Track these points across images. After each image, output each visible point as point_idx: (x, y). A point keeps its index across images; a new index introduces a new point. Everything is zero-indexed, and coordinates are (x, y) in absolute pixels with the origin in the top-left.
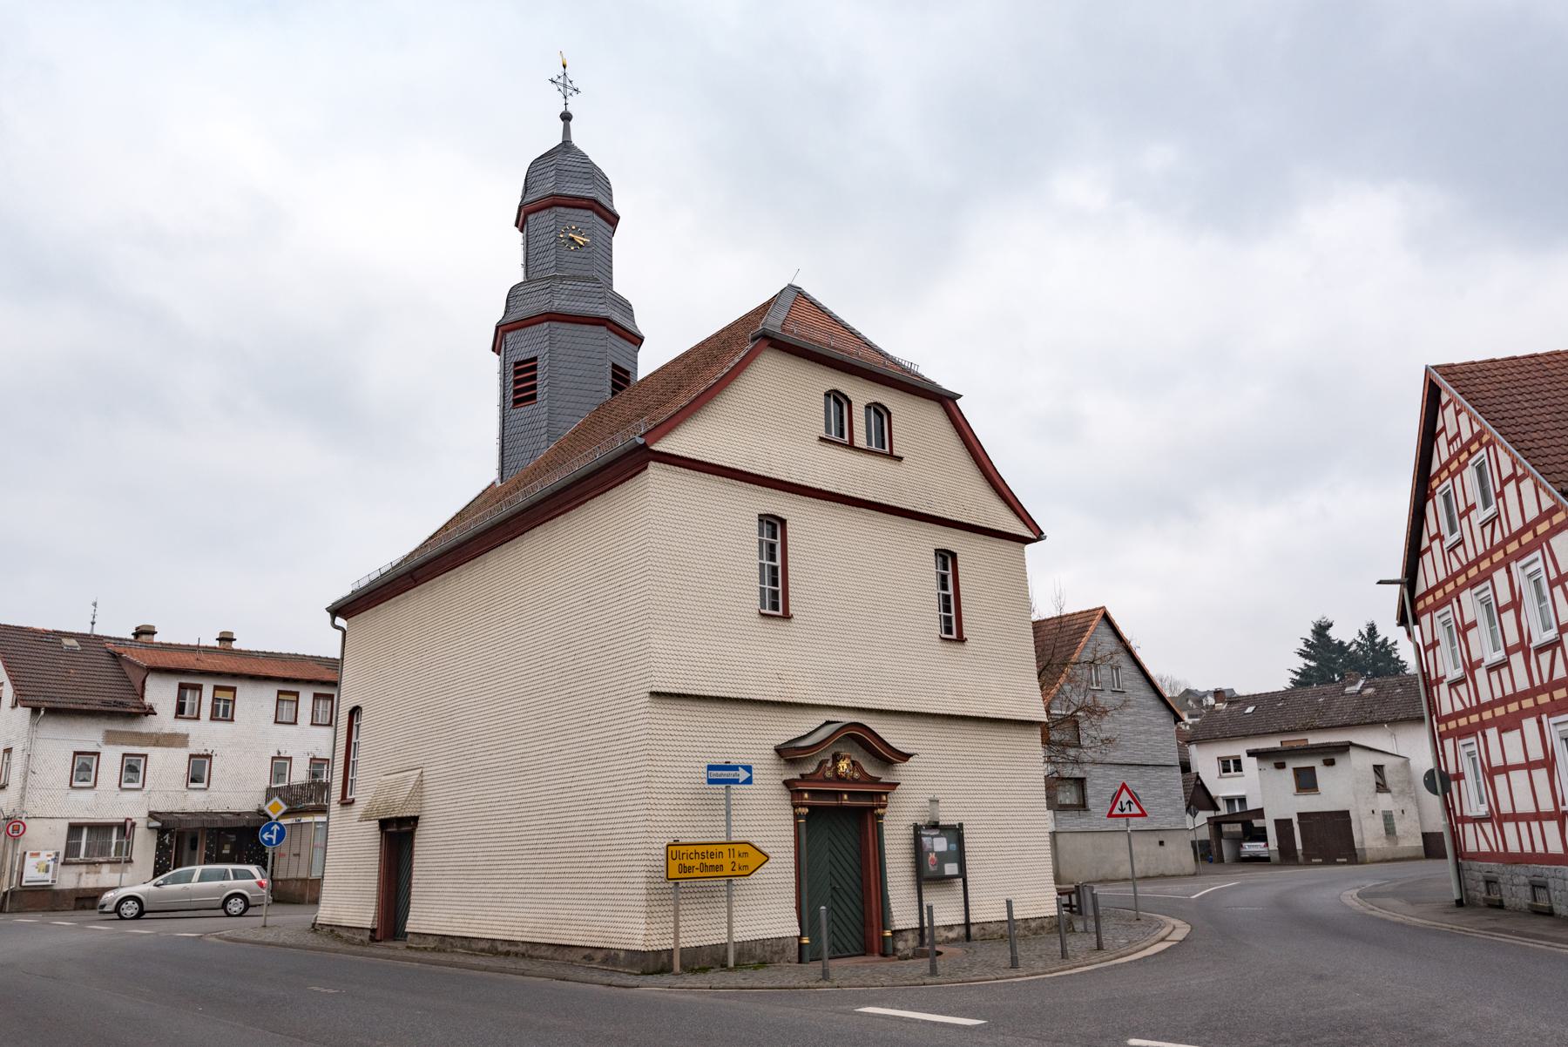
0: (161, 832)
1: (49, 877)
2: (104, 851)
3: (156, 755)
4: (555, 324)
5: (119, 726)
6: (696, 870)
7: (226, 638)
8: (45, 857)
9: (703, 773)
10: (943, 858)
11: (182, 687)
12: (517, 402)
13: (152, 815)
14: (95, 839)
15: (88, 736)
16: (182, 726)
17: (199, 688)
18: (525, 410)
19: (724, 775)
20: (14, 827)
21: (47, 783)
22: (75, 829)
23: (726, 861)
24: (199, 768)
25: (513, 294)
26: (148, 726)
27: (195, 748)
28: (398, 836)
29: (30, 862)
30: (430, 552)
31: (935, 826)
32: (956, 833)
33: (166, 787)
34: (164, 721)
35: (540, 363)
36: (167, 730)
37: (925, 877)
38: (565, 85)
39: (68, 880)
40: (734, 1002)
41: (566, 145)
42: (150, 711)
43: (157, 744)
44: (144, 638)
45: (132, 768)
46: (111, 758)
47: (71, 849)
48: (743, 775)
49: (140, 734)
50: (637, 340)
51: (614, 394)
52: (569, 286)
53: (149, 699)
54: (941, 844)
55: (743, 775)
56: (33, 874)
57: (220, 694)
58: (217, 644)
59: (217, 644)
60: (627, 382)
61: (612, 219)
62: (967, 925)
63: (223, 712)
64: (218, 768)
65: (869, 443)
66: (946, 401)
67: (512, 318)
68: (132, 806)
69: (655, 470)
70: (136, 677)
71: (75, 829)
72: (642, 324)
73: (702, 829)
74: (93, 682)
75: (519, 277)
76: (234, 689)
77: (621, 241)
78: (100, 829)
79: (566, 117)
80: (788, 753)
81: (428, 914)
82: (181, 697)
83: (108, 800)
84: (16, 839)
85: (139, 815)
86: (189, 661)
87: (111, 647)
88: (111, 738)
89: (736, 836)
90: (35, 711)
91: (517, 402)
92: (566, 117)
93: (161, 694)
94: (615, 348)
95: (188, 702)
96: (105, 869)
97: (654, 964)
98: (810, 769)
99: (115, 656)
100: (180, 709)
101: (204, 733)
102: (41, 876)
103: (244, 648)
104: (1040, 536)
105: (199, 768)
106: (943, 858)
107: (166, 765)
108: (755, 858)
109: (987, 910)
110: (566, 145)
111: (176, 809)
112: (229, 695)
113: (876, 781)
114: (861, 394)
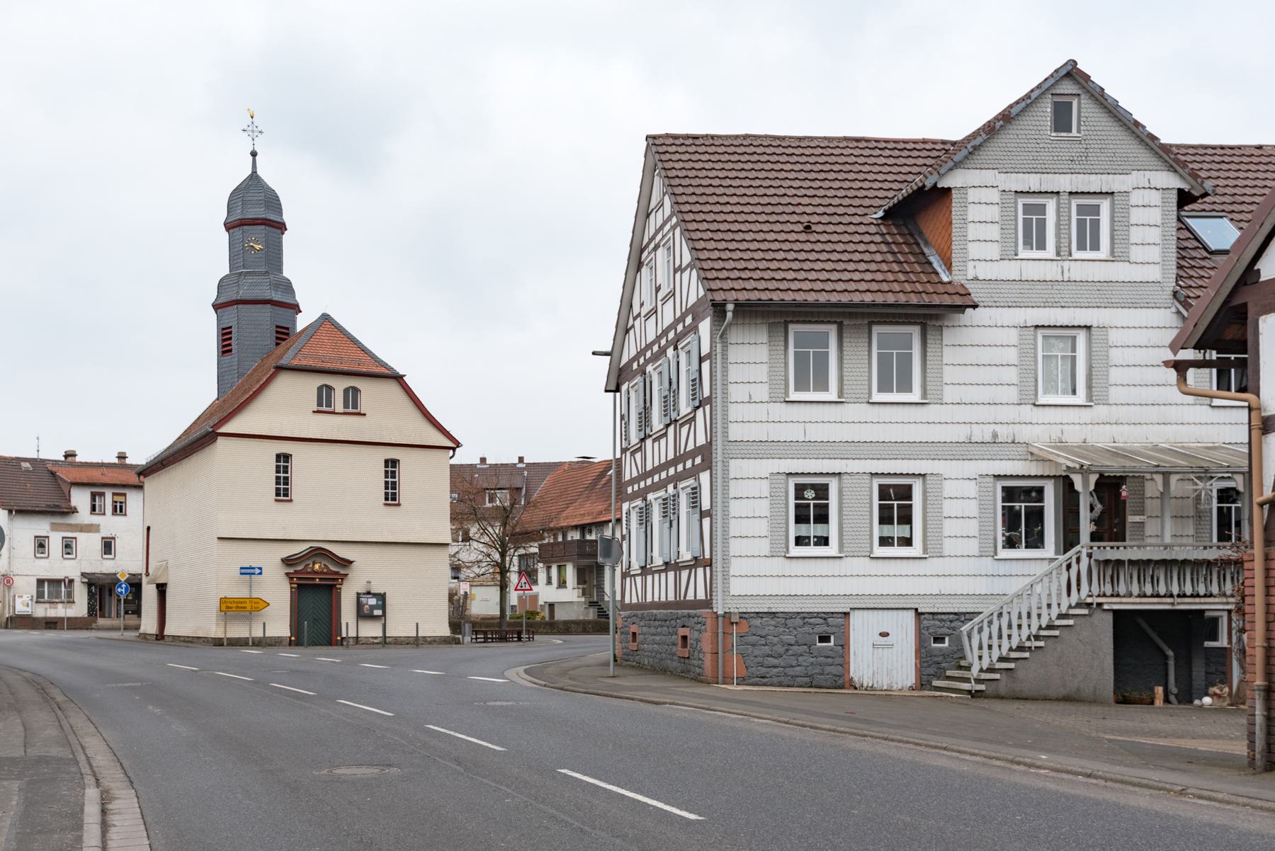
0: (90, 585)
1: (29, 609)
2: (58, 596)
3: (82, 538)
4: (240, 306)
5: (58, 520)
6: (232, 609)
7: (122, 457)
8: (26, 598)
9: (238, 571)
10: (374, 607)
11: (93, 496)
12: (224, 352)
13: (83, 575)
14: (51, 587)
15: (41, 526)
16: (95, 519)
17: (103, 494)
18: (227, 358)
19: (247, 571)
20: (7, 580)
21: (14, 559)
22: (40, 582)
23: (248, 606)
24: (108, 546)
25: (222, 285)
26: (73, 520)
27: (105, 533)
28: (162, 589)
29: (18, 601)
30: (179, 446)
31: (369, 593)
32: (382, 597)
33: (89, 558)
34: (84, 516)
35: (234, 330)
36: (86, 522)
37: (363, 614)
38: (253, 130)
39: (41, 611)
40: (850, 743)
41: (254, 176)
42: (74, 511)
43: (81, 531)
44: (70, 459)
45: (68, 547)
46: (56, 541)
47: (40, 595)
48: (258, 571)
49: (70, 525)
50: (296, 308)
51: (277, 344)
52: (250, 280)
53: (73, 503)
54: (373, 601)
55: (258, 571)
56: (21, 607)
57: (116, 498)
58: (116, 461)
59: (116, 461)
60: (291, 332)
61: (282, 227)
62: (385, 637)
63: (119, 509)
64: (119, 545)
65: (346, 406)
66: (399, 379)
67: (220, 301)
68: (70, 569)
69: (220, 439)
70: (65, 488)
71: (40, 582)
72: (300, 298)
73: (240, 592)
74: (41, 489)
75: (225, 271)
76: (125, 495)
77: (289, 241)
78: (55, 583)
79: (254, 154)
80: (287, 561)
81: (169, 630)
82: (93, 499)
83: (55, 565)
84: (9, 587)
85: (75, 574)
86: (96, 475)
87: (50, 467)
88: (55, 527)
89: (254, 596)
90: (10, 512)
91: (224, 352)
92: (254, 154)
93: (80, 499)
94: (281, 316)
95: (97, 504)
96: (60, 606)
97: (218, 643)
98: (300, 568)
99: (53, 474)
100: (93, 508)
101: (109, 524)
102: (25, 609)
103: (134, 463)
104: (458, 445)
105: (108, 546)
106: (372, 607)
107: (88, 544)
108: (261, 605)
109: (399, 626)
110: (254, 176)
111: (97, 571)
112: (121, 499)
113: (337, 573)
114: (340, 385)
